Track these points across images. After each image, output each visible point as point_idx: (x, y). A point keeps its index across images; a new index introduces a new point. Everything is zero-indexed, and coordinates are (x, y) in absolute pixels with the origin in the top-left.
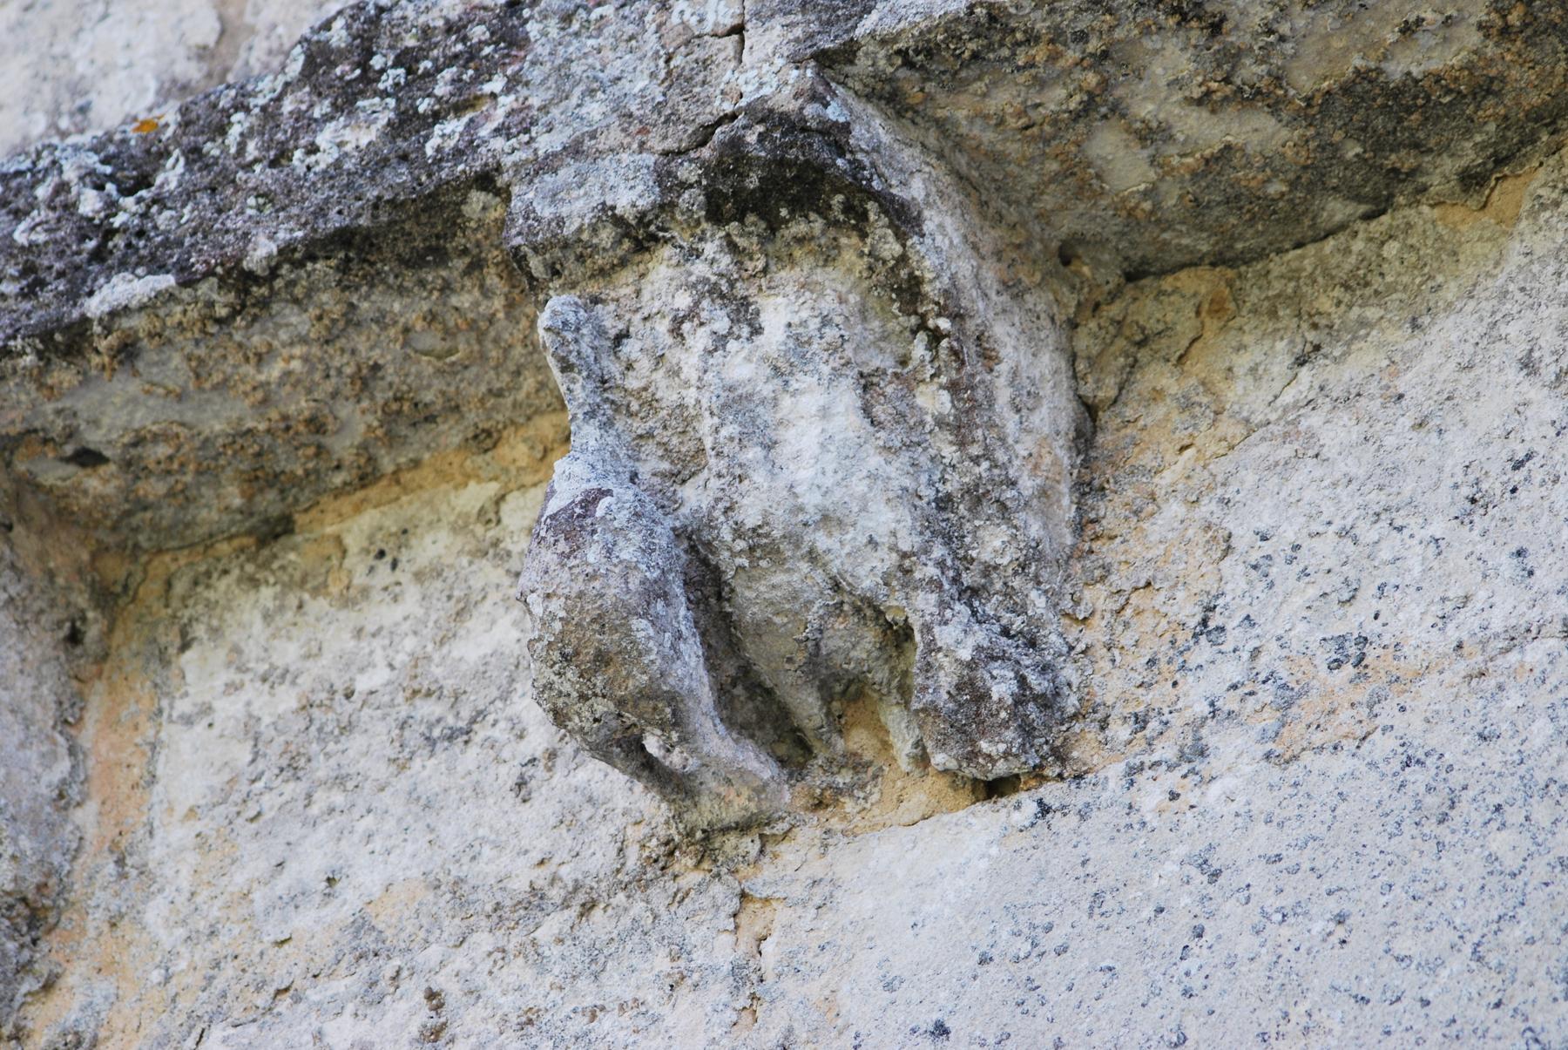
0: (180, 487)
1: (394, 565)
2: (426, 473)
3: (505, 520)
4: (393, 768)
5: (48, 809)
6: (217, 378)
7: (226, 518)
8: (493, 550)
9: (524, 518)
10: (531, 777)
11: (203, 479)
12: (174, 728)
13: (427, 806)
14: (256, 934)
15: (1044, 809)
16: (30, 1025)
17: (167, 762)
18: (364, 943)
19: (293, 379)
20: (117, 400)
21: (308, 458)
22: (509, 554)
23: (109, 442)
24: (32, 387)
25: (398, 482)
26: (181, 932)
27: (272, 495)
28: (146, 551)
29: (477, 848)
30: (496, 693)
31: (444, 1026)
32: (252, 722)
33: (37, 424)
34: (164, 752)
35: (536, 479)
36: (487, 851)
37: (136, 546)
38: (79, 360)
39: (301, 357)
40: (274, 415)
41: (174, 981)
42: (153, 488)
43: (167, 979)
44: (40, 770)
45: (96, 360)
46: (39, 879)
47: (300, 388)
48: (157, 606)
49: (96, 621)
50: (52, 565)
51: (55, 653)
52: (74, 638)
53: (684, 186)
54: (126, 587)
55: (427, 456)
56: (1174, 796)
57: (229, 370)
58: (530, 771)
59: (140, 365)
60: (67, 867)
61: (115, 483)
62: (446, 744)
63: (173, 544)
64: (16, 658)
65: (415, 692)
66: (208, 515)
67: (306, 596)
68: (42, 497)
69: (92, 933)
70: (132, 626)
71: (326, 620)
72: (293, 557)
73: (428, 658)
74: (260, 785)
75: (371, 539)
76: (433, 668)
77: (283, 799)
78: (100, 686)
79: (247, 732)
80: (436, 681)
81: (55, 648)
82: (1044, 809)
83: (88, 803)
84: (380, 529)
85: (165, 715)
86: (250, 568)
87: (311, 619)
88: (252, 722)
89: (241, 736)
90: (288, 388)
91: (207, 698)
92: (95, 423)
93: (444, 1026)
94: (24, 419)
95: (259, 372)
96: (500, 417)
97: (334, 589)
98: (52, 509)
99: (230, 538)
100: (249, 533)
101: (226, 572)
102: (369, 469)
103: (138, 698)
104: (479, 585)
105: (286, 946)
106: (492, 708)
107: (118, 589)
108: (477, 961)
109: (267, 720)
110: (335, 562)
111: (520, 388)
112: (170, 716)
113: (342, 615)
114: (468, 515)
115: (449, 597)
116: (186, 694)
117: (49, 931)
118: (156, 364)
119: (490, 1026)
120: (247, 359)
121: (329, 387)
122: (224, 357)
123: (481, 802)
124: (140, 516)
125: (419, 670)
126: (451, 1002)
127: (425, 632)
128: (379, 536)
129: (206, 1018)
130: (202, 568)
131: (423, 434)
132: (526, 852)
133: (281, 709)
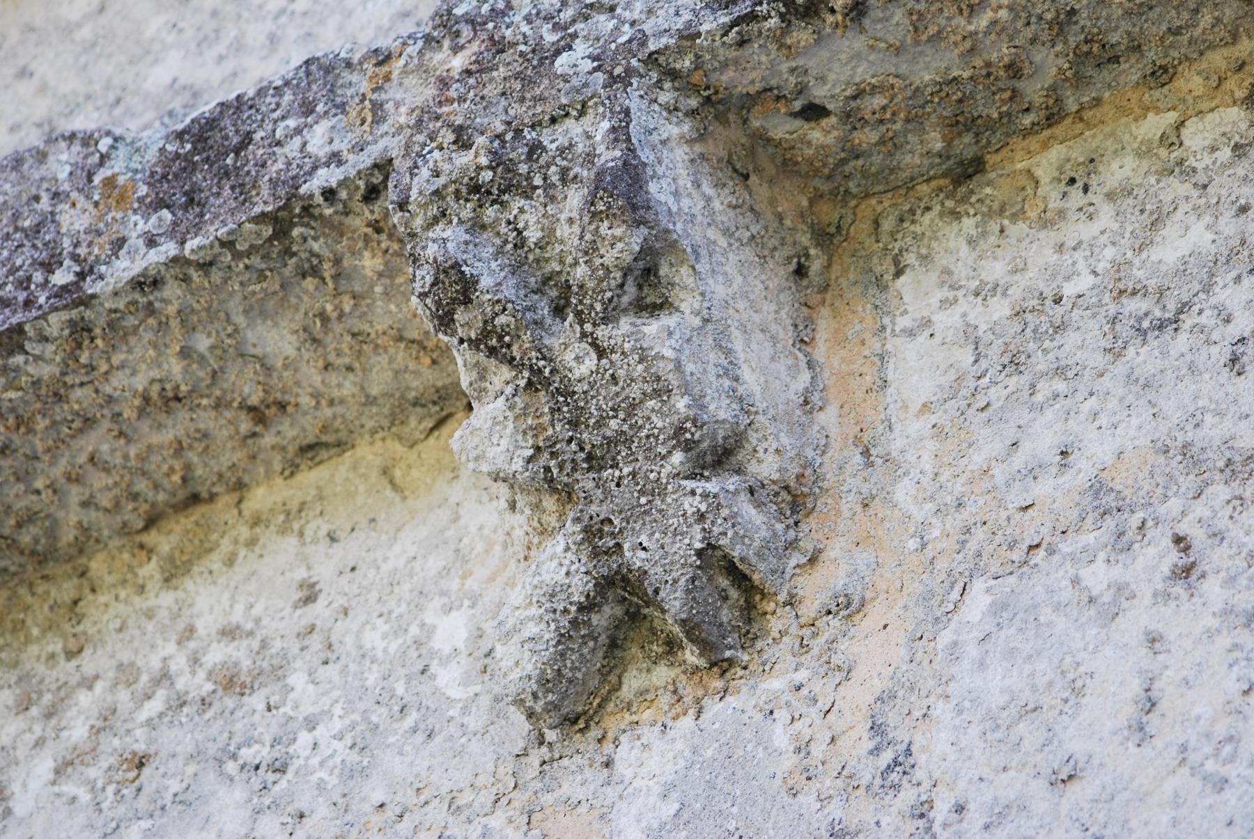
0: (890, 134)
1: (1086, 189)
2: (1107, 109)
3: (1187, 143)
4: (1109, 357)
5: (798, 412)
6: (932, 30)
7: (926, 162)
8: (1180, 168)
9: (1204, 139)
10: (1243, 354)
11: (909, 127)
12: (897, 341)
13: (1145, 386)
14: (1001, 504)
16: (801, 593)
17: (896, 369)
18: (1103, 500)
19: (998, 28)
20: (843, 57)
21: (1004, 102)
22: (1194, 170)
23: (833, 96)
24: (773, 47)
25: (1081, 119)
26: (930, 506)
27: (968, 138)
28: (855, 196)
29: (1199, 416)
30: (1197, 287)
31: (1193, 564)
32: (970, 330)
33: (773, 83)
34: (892, 360)
35: (1213, 105)
36: (1209, 418)
37: (847, 191)
38: (816, 21)
39: (1007, 7)
40: (978, 62)
41: (929, 547)
42: (867, 137)
43: (924, 546)
44: (788, 380)
45: (830, 19)
46: (797, 470)
47: (1003, 36)
48: (869, 242)
49: (817, 256)
50: (780, 209)
51: (788, 284)
52: (800, 272)
54: (839, 227)
55: (1107, 94)
57: (943, 22)
58: (1240, 349)
59: (867, 22)
60: (819, 460)
61: (835, 133)
62: (1157, 333)
63: (880, 188)
64: (761, 286)
65: (1121, 292)
66: (911, 160)
67: (1006, 222)
68: (771, 150)
69: (846, 514)
70: (847, 260)
71: (1028, 240)
72: (988, 191)
73: (1129, 263)
74: (985, 380)
75: (1061, 170)
76: (1135, 271)
77: (1009, 390)
78: (825, 311)
79: (967, 338)
80: (1140, 281)
81: (787, 279)
83: (829, 407)
84: (1069, 160)
85: (889, 330)
86: (950, 204)
87: (1013, 241)
88: (970, 330)
89: (962, 341)
90: (993, 36)
91: (925, 313)
92: (822, 79)
93: (1193, 564)
94: (763, 79)
95: (970, 23)
96: (1176, 54)
97: (1032, 214)
98: (779, 160)
99: (928, 181)
100: (945, 175)
101: (928, 209)
102: (1056, 110)
103: (861, 318)
104: (1170, 198)
105: (1030, 511)
106: (1196, 299)
107: (832, 230)
108: (1217, 509)
109: (983, 327)
110: (1029, 191)
111: (1198, 25)
112: (893, 330)
113: (1042, 234)
114: (1150, 141)
115: (1142, 211)
116: (906, 312)
117: (808, 515)
118: (880, 20)
119: (1237, 562)
120: (961, 11)
121: (1028, 33)
122: (941, 10)
123: (1198, 378)
124: (852, 164)
125: (1122, 274)
126: (1196, 544)
127: (1122, 242)
128: (1068, 166)
129: (967, 574)
130: (907, 207)
131: (1106, 74)
132: (1247, 416)
133: (995, 317)
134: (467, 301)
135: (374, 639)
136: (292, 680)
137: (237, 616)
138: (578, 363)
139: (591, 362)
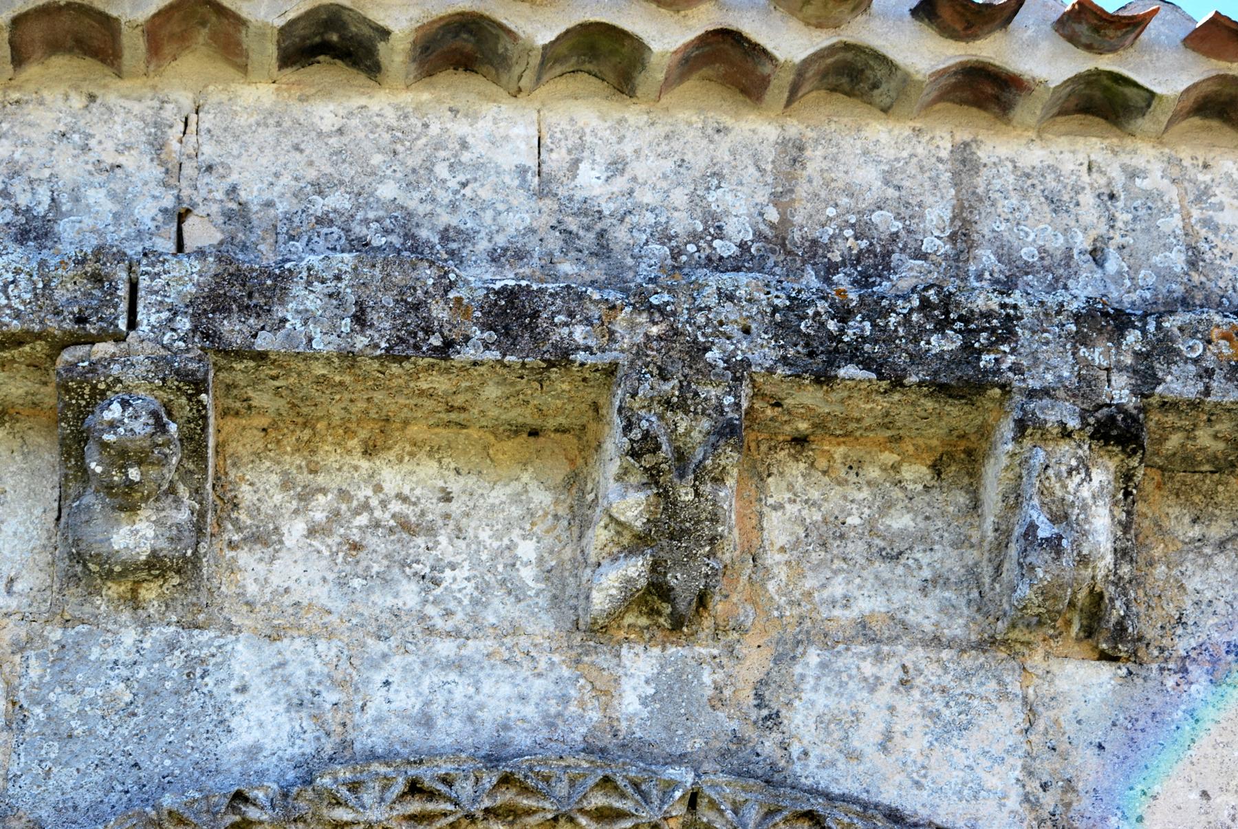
15: (1130, 673)
36: (912, 612)
53: (1089, 424)
56: (1178, 685)
82: (1130, 673)
86: (793, 451)
134: (654, 453)
135: (484, 535)
136: (440, 538)
137: (406, 491)
138: (686, 495)
139: (691, 497)
